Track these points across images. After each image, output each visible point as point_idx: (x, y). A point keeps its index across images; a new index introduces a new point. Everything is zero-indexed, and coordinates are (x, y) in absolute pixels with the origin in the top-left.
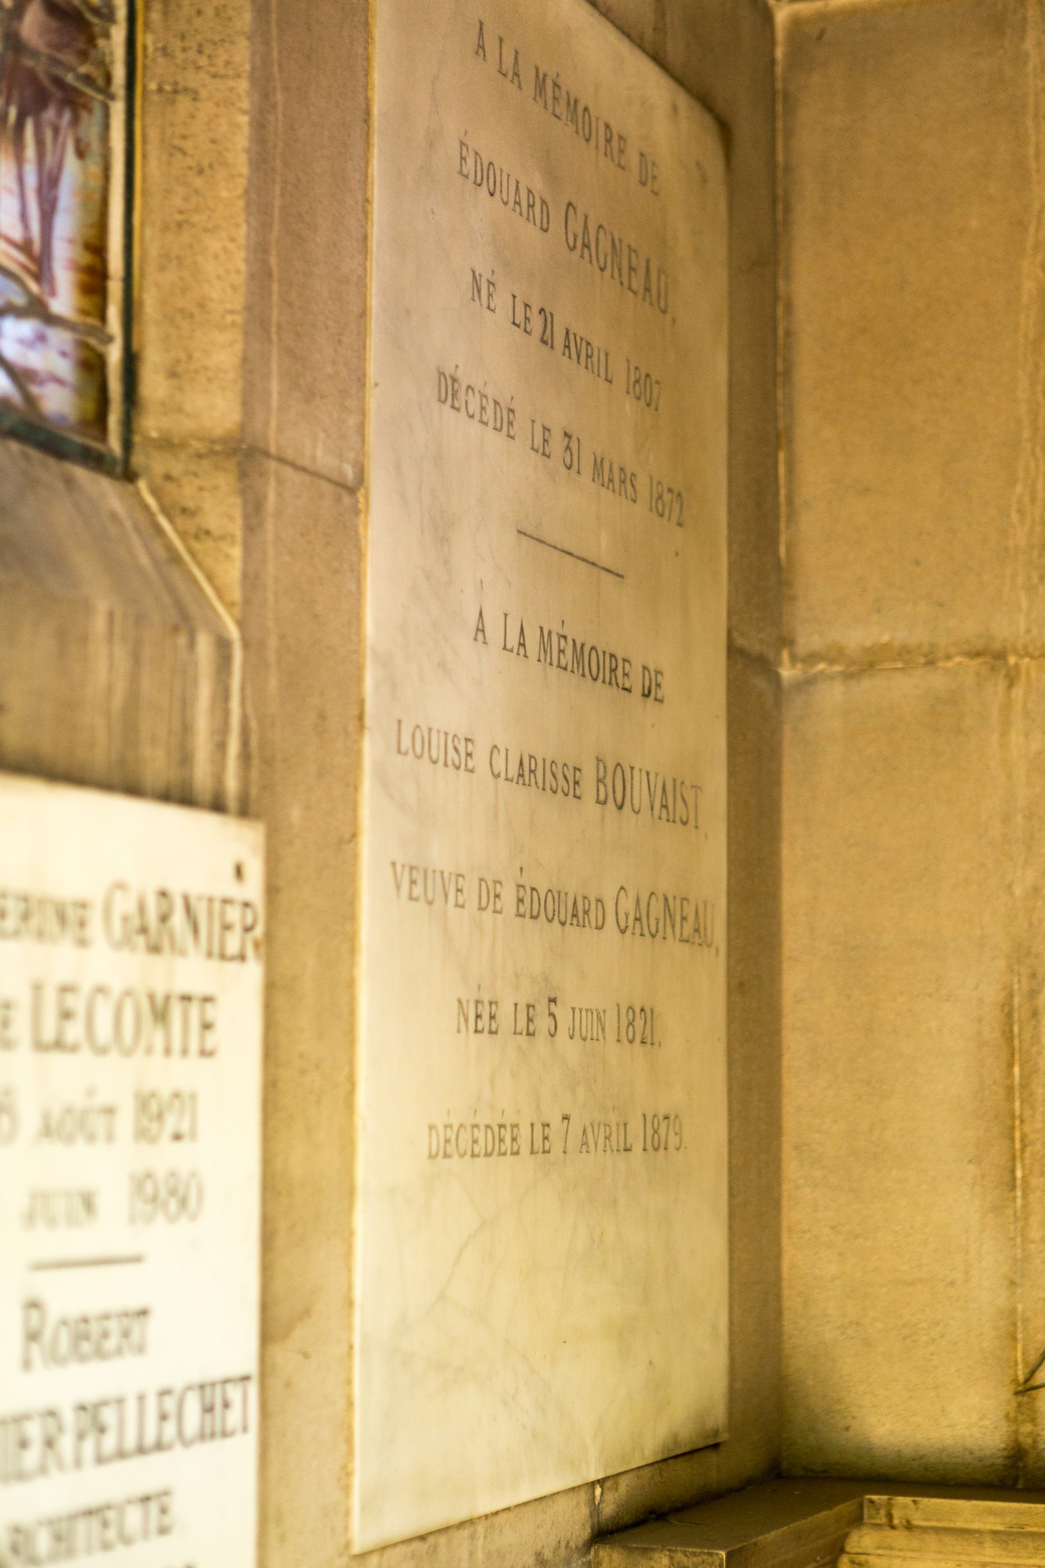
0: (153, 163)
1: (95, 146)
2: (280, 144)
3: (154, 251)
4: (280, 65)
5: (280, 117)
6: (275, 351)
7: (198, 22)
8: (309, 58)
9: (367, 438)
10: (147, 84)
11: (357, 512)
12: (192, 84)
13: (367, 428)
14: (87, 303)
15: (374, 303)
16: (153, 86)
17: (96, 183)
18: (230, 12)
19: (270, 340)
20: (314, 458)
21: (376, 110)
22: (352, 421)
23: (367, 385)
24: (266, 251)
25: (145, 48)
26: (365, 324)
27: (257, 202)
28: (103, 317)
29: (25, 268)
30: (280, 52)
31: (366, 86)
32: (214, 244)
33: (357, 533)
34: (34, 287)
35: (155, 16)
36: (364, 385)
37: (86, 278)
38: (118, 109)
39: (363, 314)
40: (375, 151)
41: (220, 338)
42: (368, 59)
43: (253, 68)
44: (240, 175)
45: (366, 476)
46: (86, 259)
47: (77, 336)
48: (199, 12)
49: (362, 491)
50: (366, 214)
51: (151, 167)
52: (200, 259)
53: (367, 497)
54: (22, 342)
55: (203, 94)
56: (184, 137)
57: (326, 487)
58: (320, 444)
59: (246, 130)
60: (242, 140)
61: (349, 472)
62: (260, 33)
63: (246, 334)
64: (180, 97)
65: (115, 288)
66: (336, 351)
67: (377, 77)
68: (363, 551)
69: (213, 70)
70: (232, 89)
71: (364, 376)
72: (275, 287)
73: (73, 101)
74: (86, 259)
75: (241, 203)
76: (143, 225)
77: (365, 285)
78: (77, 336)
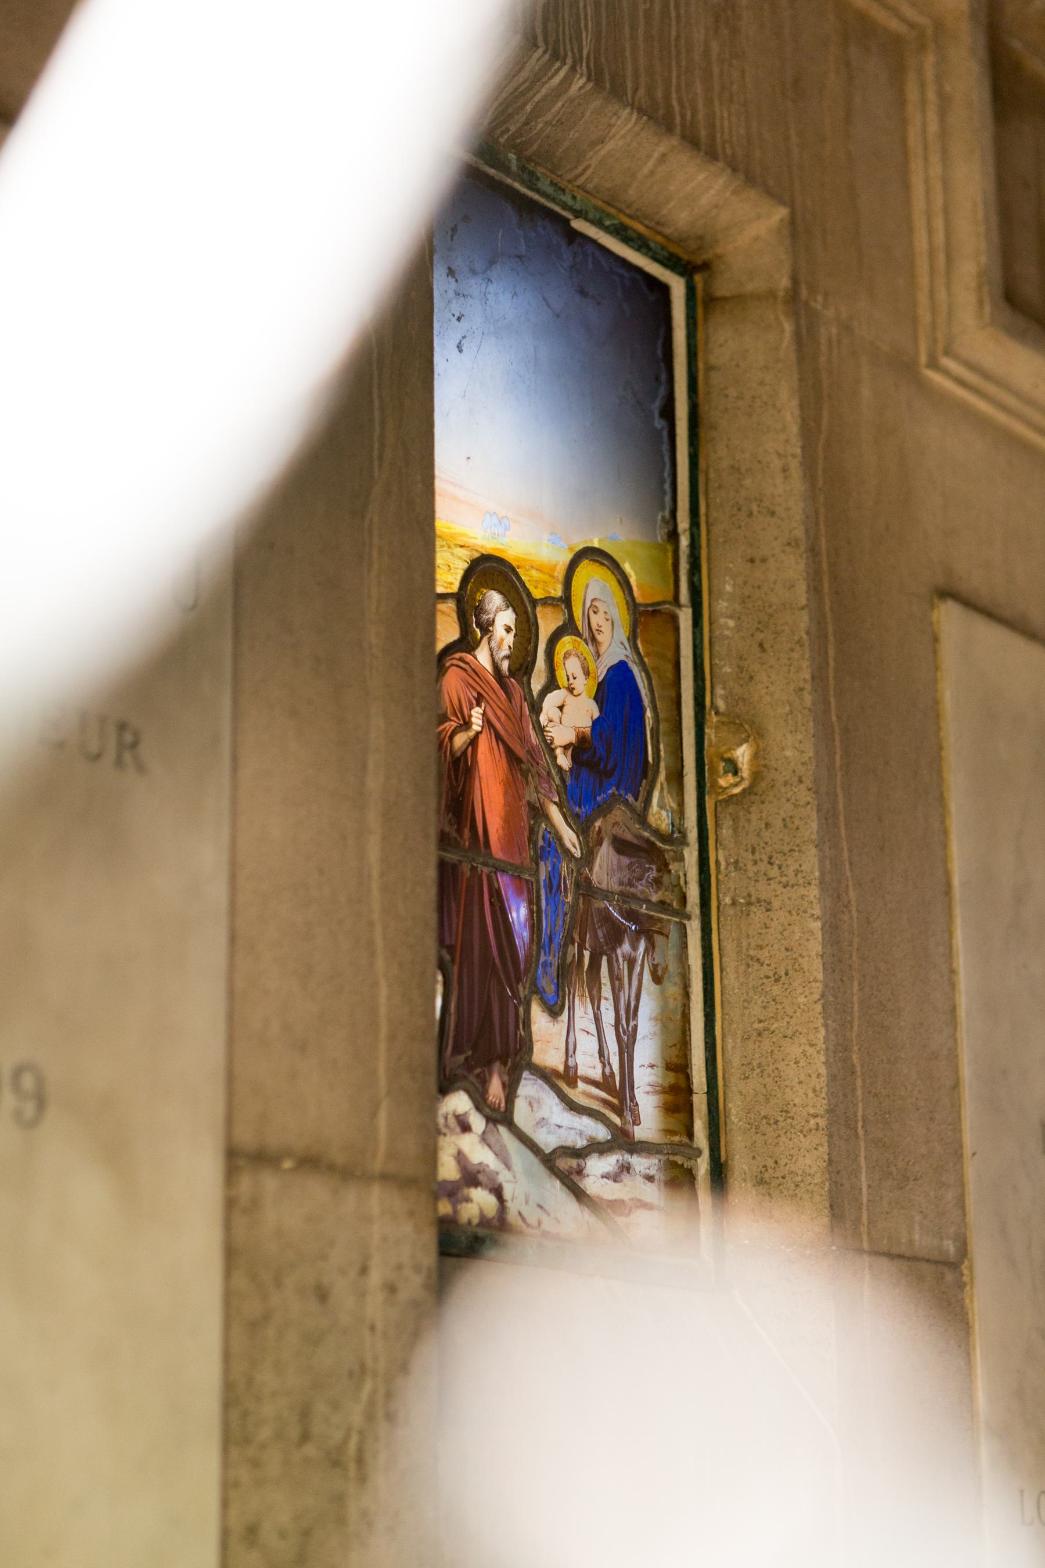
0: (731, 977)
1: (673, 967)
2: (856, 940)
3: (736, 1061)
4: (851, 864)
5: (855, 914)
6: (862, 1144)
7: (766, 834)
8: (882, 848)
9: (967, 1210)
10: (722, 897)
11: (961, 1286)
12: (763, 896)
13: (967, 1199)
14: (674, 1123)
15: (966, 1072)
16: (728, 900)
17: (675, 1004)
18: (797, 822)
19: (857, 1136)
20: (911, 1242)
21: (956, 882)
22: (950, 1195)
23: (965, 1156)
24: (847, 1049)
25: (717, 862)
26: (959, 1093)
27: (835, 1005)
28: (690, 1135)
29: (605, 1102)
30: (850, 851)
31: (945, 860)
32: (794, 1050)
33: (963, 1307)
34: (617, 1120)
35: (726, 832)
36: (962, 1156)
37: (669, 1098)
38: (694, 928)
39: (956, 1086)
40: (958, 922)
41: (805, 1143)
42: (945, 832)
43: (822, 874)
44: (816, 981)
45: (969, 1247)
46: (671, 1078)
47: (663, 1158)
48: (767, 825)
49: (966, 1263)
50: (953, 986)
51: (730, 980)
52: (781, 1066)
53: (971, 1269)
54: (606, 1176)
55: (776, 904)
56: (761, 947)
57: (924, 1266)
58: (916, 1226)
59: (819, 935)
60: (815, 946)
61: (950, 1247)
62: (829, 838)
63: (830, 1136)
64: (753, 908)
65: (700, 1102)
66: (928, 1129)
67: (955, 848)
68: (971, 1324)
69: (784, 879)
70: (803, 897)
71: (961, 1147)
72: (859, 1082)
73: (648, 931)
74: (671, 1078)
75: (819, 1007)
76: (724, 1036)
77: (957, 1056)
78: (663, 1158)
